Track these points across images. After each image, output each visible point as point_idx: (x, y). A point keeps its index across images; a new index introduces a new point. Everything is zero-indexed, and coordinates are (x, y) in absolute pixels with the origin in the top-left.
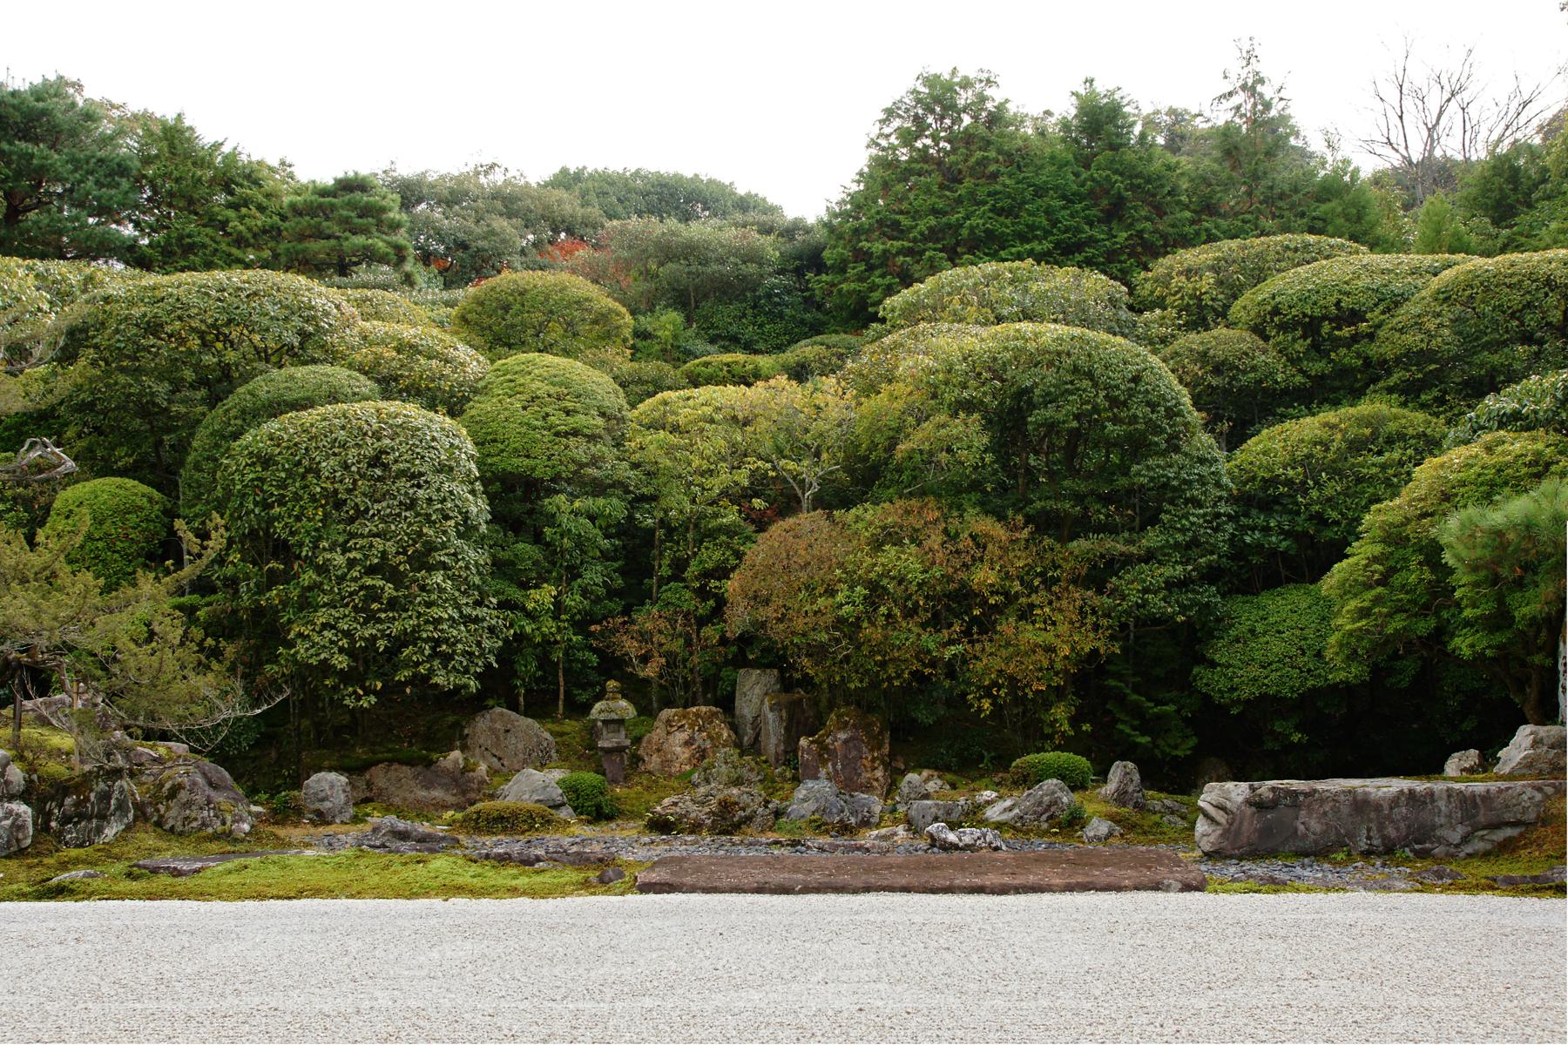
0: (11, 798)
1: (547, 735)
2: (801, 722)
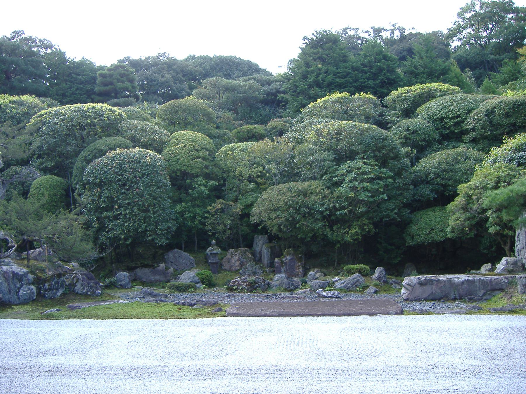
0: (30, 284)
1: (192, 258)
2: (276, 253)
